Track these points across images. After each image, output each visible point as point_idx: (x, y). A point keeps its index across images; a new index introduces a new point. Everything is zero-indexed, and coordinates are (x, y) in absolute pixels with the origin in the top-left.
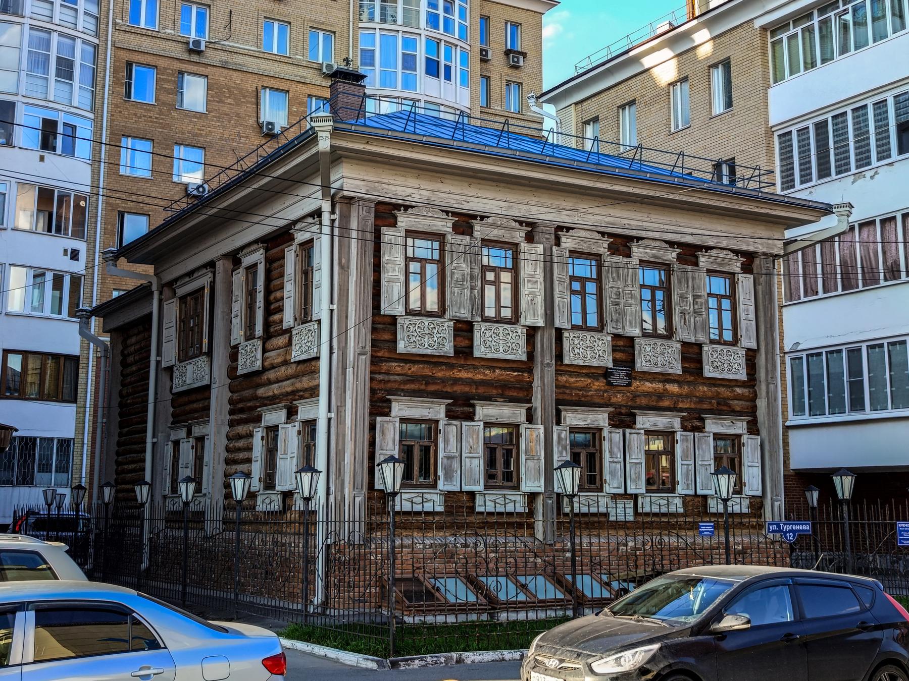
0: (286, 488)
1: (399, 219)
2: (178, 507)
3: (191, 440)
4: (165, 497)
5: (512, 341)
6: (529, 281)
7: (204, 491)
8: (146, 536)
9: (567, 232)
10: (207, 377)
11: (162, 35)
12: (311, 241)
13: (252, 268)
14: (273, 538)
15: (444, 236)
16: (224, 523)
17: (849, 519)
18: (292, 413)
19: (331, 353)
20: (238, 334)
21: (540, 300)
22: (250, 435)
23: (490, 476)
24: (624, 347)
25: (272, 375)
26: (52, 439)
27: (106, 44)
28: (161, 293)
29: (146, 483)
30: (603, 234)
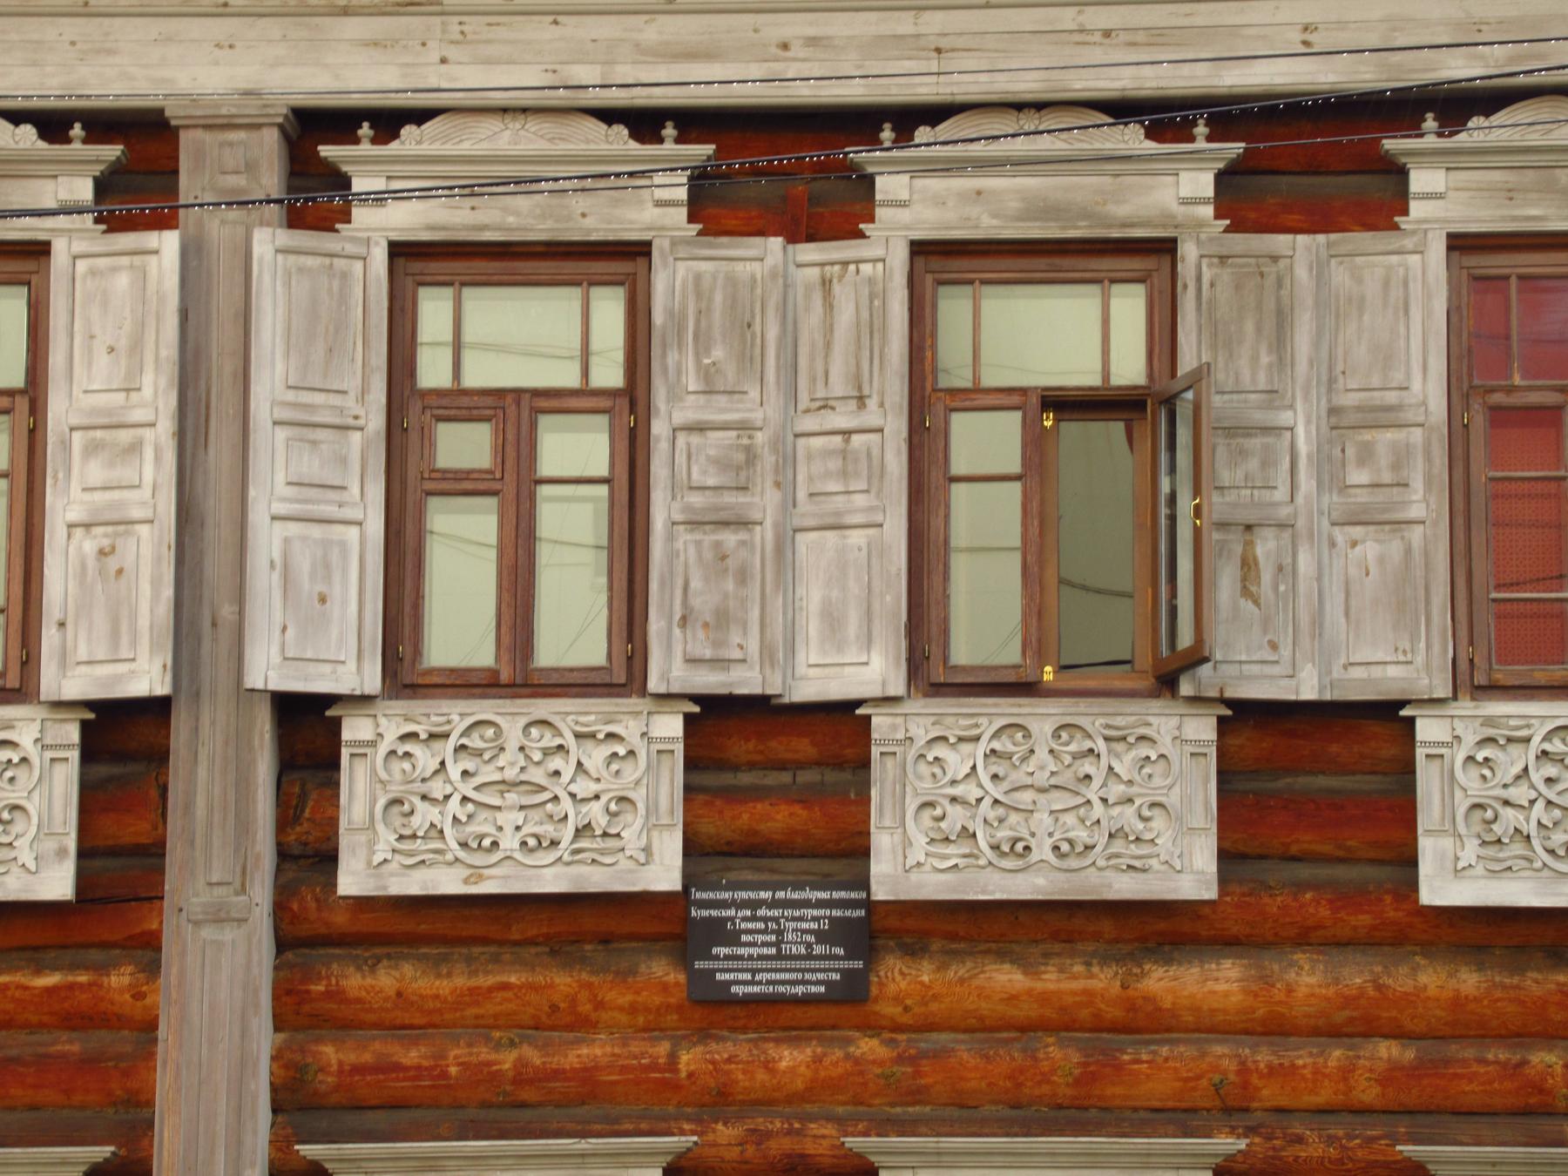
5: (583, 787)
6: (92, 449)
9: (904, 136)
15: (1166, 248)
21: (149, 552)
24: (773, 767)
30: (644, 123)
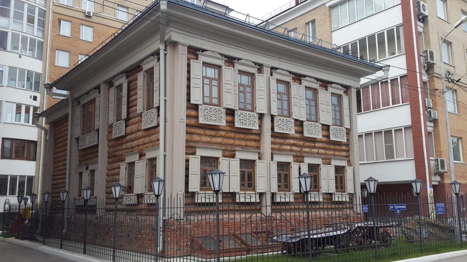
0: (139, 193)
1: (199, 56)
2: (82, 203)
3: (88, 171)
4: (75, 199)
7: (95, 195)
8: (66, 216)
10: (96, 141)
11: (74, 9)
12: (153, 68)
13: (120, 87)
14: (136, 218)
16: (105, 210)
17: (375, 203)
18: (141, 155)
19: (165, 122)
20: (112, 118)
22: (119, 168)
23: (242, 185)
25: (129, 137)
26: (25, 176)
27: (50, 10)
28: (73, 103)
29: (66, 191)
